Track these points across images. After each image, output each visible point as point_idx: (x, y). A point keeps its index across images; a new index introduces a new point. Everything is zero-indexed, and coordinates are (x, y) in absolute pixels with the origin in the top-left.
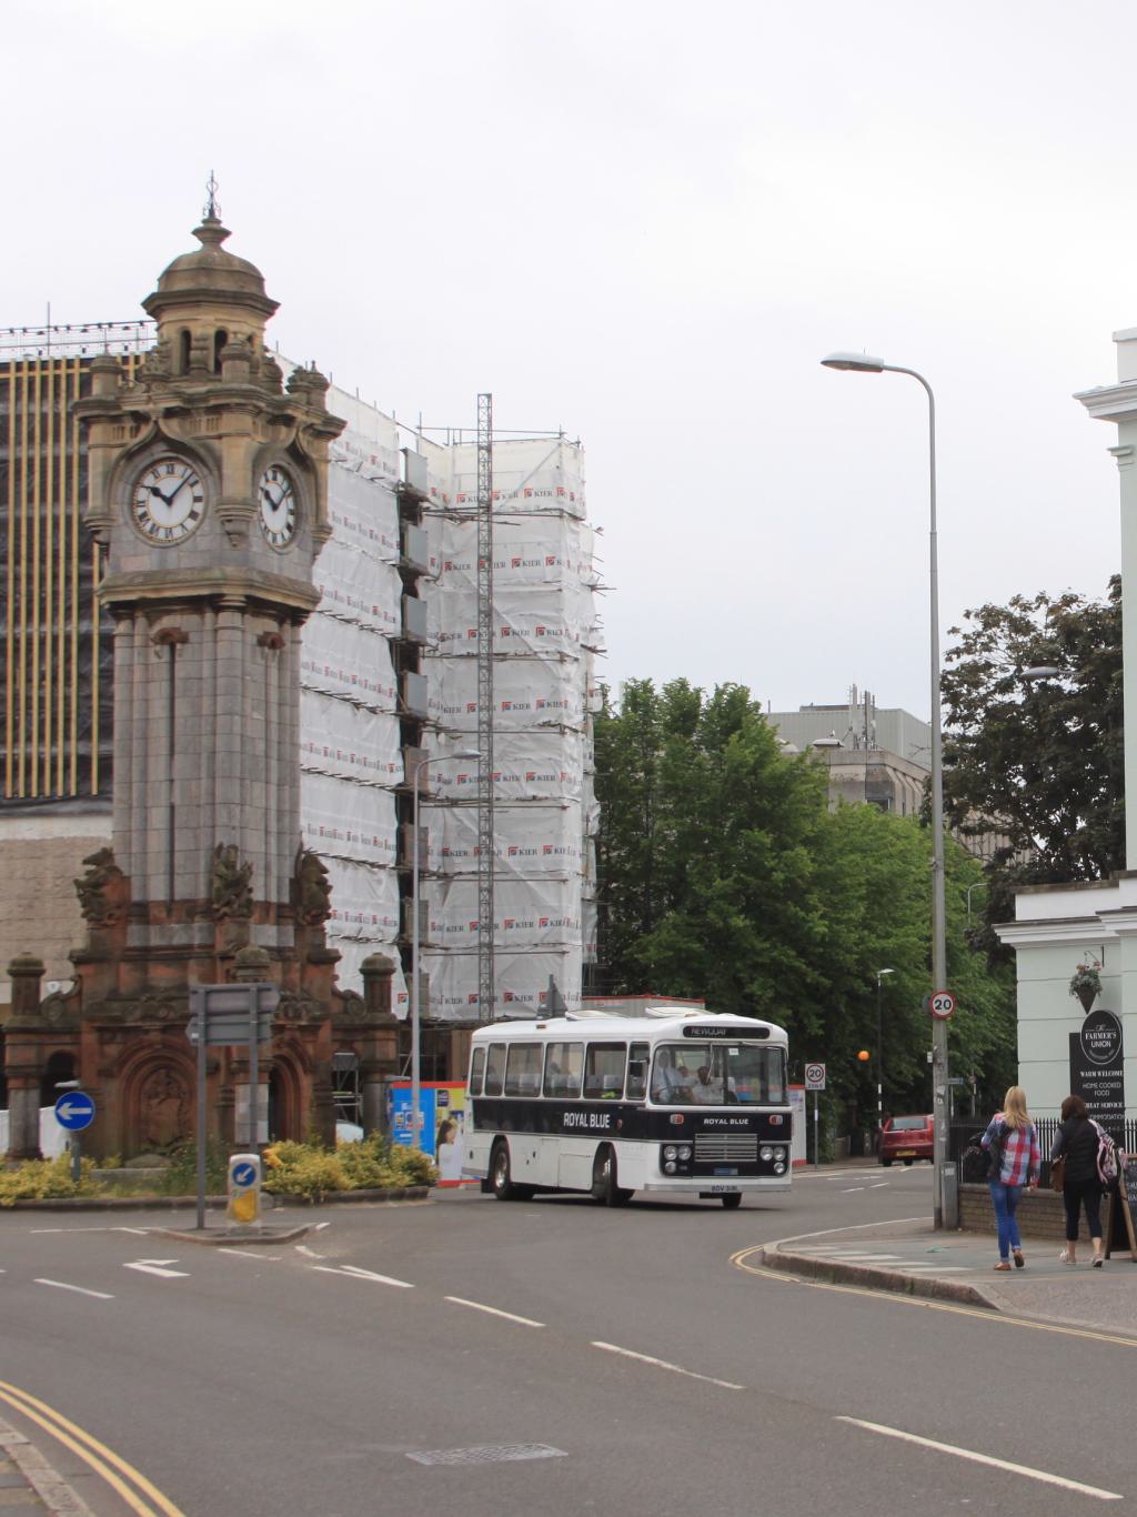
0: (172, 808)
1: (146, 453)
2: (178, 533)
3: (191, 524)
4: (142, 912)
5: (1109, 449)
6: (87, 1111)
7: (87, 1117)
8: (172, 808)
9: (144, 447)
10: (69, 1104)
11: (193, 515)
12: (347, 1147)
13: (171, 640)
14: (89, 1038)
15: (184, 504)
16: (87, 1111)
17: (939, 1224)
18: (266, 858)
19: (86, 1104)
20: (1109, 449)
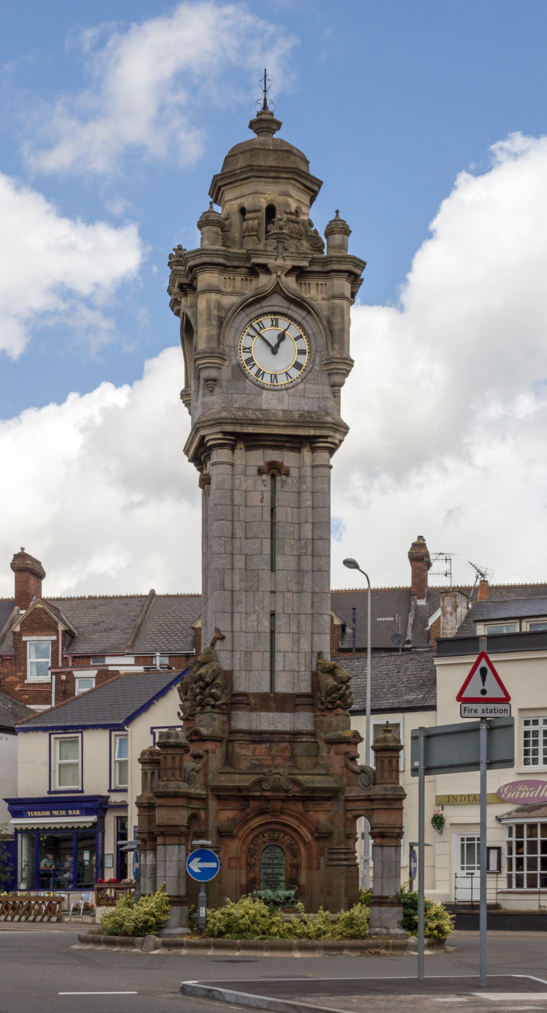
0: (273, 569)
1: (258, 306)
2: (282, 380)
3: (295, 373)
4: (239, 701)
5: (6, 800)
6: (213, 865)
7: (214, 870)
8: (273, 569)
9: (259, 299)
10: (199, 859)
11: (297, 366)
12: (202, 625)
13: (274, 470)
14: (70, 914)
15: (290, 350)
16: (213, 865)
17: (347, 834)
18: (156, 858)
19: (213, 860)
20: (6, 800)
